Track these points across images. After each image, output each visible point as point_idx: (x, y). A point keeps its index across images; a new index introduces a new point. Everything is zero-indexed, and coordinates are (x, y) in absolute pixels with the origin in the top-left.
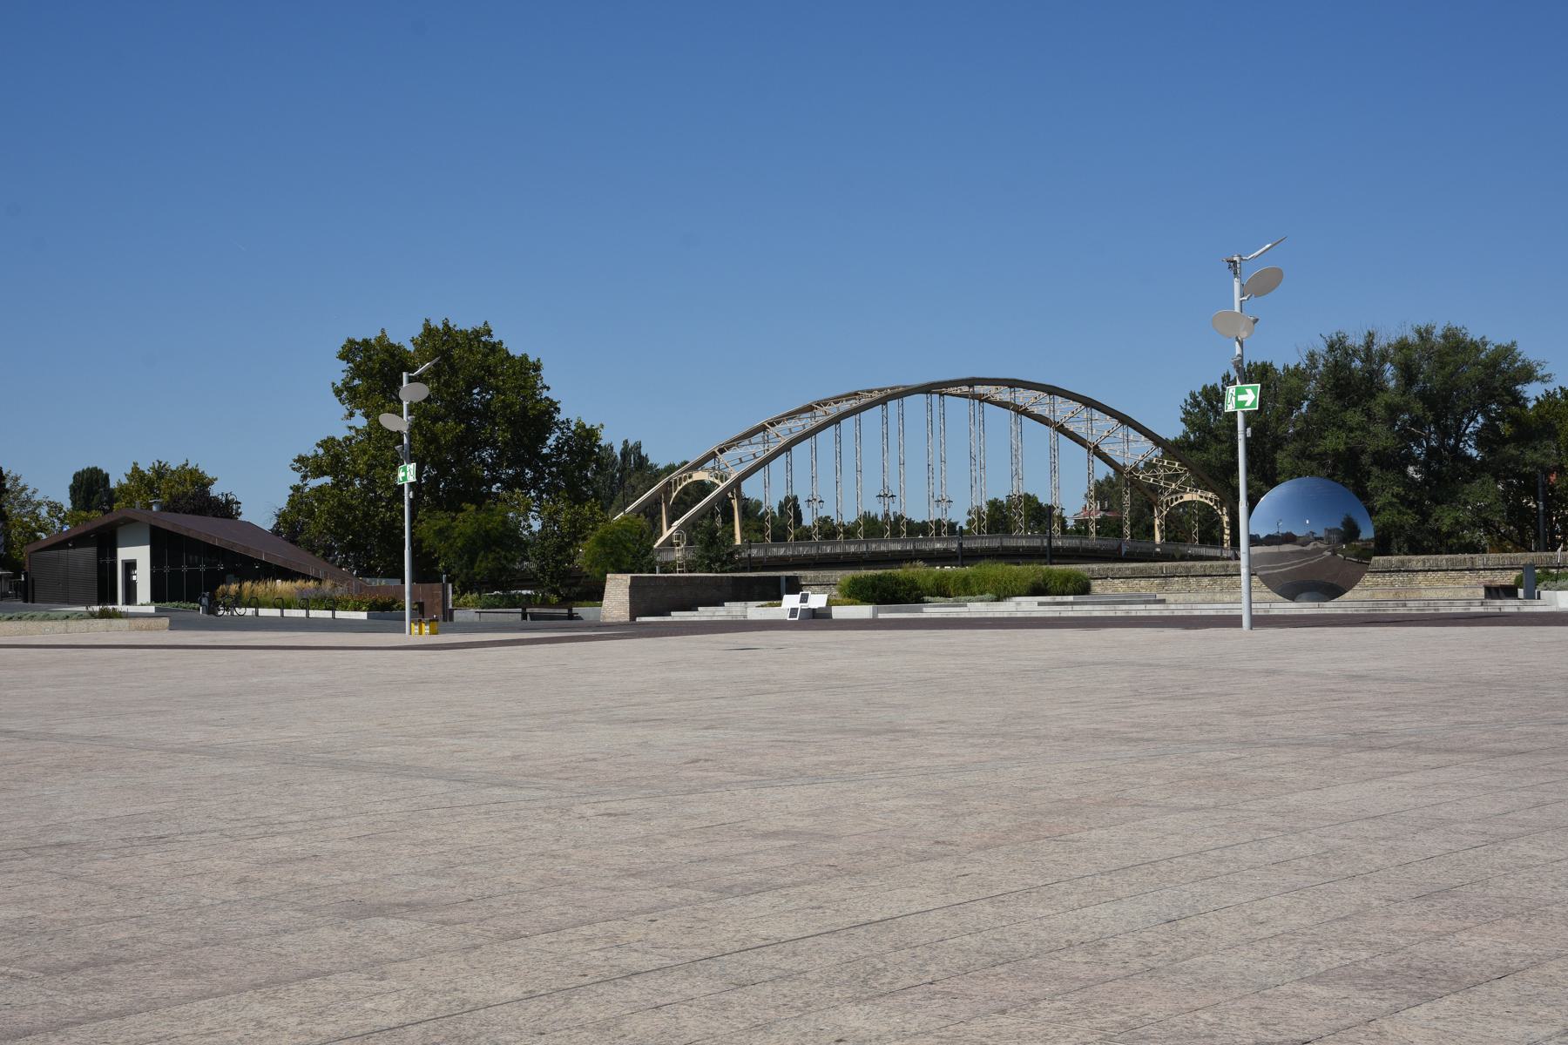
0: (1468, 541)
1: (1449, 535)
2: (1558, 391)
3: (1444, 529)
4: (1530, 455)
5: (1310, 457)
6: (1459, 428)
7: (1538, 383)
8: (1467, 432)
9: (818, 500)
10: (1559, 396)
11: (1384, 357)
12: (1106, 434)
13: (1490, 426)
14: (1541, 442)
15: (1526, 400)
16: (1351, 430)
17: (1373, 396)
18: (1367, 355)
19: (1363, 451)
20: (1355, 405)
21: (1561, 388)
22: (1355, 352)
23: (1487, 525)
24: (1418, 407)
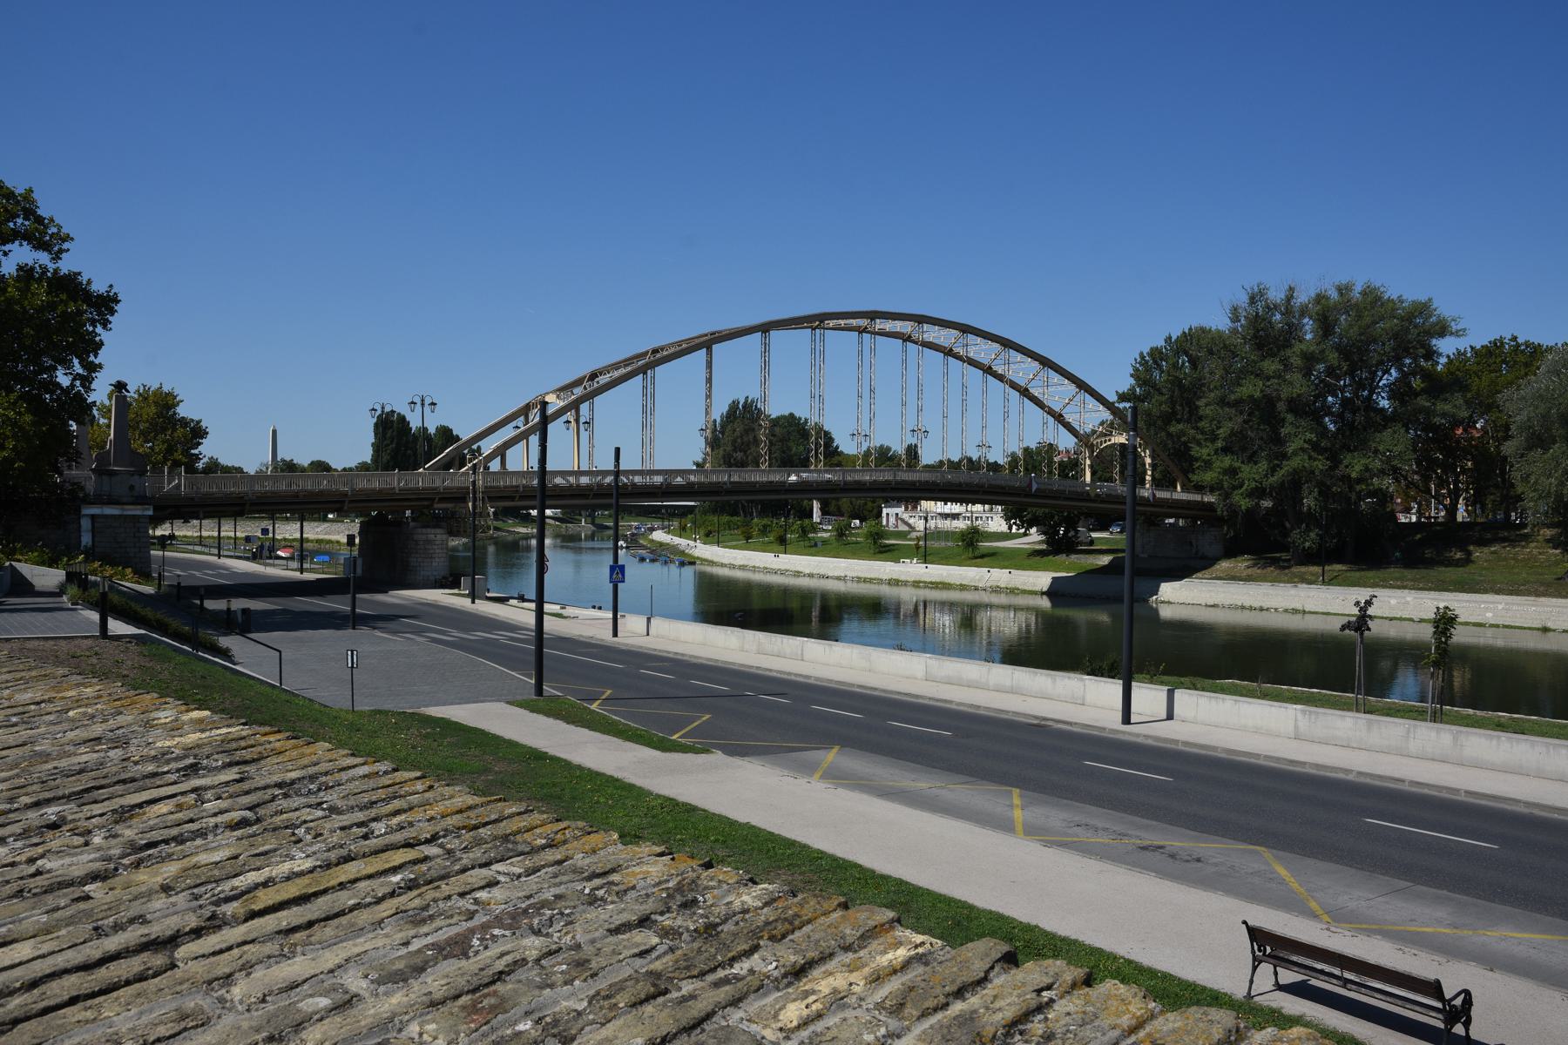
0: (1376, 487)
1: (1359, 481)
2: (1469, 350)
3: (1354, 475)
4: (1442, 407)
5: (1229, 405)
6: (1373, 381)
7: (1453, 338)
8: (1381, 384)
9: (863, 433)
10: (1469, 355)
11: (1304, 311)
12: (1031, 377)
13: (1404, 377)
14: (1452, 394)
15: (1440, 355)
16: (1268, 379)
17: (1291, 346)
18: (1287, 308)
19: (1279, 399)
20: (1274, 355)
21: (1471, 347)
22: (1276, 307)
23: (1396, 472)
24: (1333, 357)
